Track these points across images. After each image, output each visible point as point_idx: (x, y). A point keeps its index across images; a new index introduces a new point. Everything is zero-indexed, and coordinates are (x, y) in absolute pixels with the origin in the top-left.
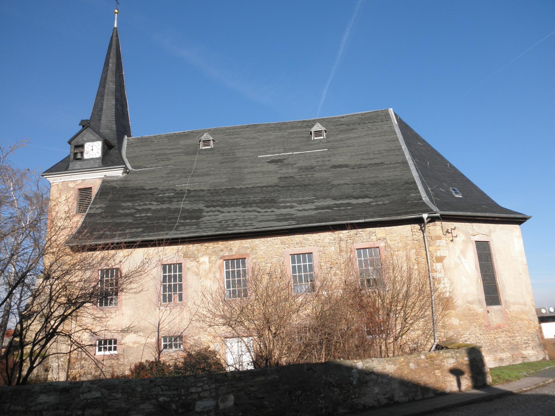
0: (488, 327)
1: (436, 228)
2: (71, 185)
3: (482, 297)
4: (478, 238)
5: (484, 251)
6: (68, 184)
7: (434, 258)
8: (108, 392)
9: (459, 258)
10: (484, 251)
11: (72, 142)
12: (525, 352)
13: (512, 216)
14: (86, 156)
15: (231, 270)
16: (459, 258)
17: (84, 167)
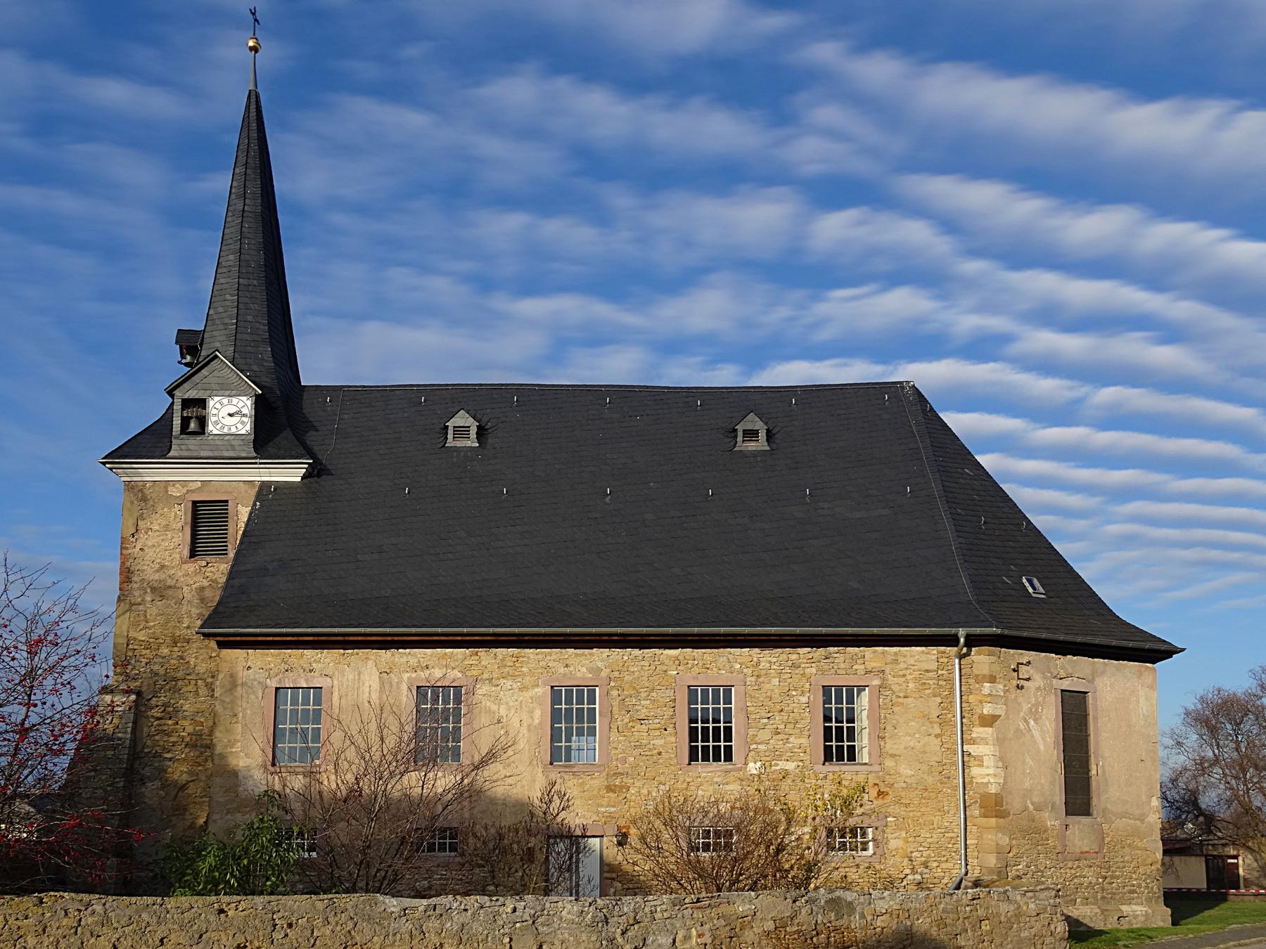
0: (1062, 855)
1: (982, 659)
2: (175, 492)
3: (1059, 798)
4: (1066, 684)
5: (1075, 712)
6: (166, 488)
7: (976, 717)
8: (990, 730)
9: (1026, 721)
10: (1075, 712)
11: (177, 393)
12: (1125, 909)
13: (1148, 646)
14: (211, 428)
15: (699, 706)
16: (1026, 721)
17: (203, 454)
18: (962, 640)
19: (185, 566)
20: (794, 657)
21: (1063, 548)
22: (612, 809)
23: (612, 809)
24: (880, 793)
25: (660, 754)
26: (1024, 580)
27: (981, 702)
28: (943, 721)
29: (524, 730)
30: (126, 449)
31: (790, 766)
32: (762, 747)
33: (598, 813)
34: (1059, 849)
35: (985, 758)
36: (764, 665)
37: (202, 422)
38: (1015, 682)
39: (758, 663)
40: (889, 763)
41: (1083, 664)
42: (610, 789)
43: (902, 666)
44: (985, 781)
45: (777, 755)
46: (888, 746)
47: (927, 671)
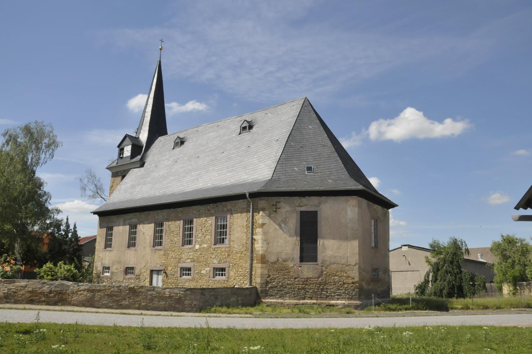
4: (303, 209)
8: (261, 229)
20: (209, 207)
24: (228, 255)
36: (201, 211)
40: (231, 243)
41: (315, 200)
42: (164, 255)
43: (237, 207)
45: (202, 242)
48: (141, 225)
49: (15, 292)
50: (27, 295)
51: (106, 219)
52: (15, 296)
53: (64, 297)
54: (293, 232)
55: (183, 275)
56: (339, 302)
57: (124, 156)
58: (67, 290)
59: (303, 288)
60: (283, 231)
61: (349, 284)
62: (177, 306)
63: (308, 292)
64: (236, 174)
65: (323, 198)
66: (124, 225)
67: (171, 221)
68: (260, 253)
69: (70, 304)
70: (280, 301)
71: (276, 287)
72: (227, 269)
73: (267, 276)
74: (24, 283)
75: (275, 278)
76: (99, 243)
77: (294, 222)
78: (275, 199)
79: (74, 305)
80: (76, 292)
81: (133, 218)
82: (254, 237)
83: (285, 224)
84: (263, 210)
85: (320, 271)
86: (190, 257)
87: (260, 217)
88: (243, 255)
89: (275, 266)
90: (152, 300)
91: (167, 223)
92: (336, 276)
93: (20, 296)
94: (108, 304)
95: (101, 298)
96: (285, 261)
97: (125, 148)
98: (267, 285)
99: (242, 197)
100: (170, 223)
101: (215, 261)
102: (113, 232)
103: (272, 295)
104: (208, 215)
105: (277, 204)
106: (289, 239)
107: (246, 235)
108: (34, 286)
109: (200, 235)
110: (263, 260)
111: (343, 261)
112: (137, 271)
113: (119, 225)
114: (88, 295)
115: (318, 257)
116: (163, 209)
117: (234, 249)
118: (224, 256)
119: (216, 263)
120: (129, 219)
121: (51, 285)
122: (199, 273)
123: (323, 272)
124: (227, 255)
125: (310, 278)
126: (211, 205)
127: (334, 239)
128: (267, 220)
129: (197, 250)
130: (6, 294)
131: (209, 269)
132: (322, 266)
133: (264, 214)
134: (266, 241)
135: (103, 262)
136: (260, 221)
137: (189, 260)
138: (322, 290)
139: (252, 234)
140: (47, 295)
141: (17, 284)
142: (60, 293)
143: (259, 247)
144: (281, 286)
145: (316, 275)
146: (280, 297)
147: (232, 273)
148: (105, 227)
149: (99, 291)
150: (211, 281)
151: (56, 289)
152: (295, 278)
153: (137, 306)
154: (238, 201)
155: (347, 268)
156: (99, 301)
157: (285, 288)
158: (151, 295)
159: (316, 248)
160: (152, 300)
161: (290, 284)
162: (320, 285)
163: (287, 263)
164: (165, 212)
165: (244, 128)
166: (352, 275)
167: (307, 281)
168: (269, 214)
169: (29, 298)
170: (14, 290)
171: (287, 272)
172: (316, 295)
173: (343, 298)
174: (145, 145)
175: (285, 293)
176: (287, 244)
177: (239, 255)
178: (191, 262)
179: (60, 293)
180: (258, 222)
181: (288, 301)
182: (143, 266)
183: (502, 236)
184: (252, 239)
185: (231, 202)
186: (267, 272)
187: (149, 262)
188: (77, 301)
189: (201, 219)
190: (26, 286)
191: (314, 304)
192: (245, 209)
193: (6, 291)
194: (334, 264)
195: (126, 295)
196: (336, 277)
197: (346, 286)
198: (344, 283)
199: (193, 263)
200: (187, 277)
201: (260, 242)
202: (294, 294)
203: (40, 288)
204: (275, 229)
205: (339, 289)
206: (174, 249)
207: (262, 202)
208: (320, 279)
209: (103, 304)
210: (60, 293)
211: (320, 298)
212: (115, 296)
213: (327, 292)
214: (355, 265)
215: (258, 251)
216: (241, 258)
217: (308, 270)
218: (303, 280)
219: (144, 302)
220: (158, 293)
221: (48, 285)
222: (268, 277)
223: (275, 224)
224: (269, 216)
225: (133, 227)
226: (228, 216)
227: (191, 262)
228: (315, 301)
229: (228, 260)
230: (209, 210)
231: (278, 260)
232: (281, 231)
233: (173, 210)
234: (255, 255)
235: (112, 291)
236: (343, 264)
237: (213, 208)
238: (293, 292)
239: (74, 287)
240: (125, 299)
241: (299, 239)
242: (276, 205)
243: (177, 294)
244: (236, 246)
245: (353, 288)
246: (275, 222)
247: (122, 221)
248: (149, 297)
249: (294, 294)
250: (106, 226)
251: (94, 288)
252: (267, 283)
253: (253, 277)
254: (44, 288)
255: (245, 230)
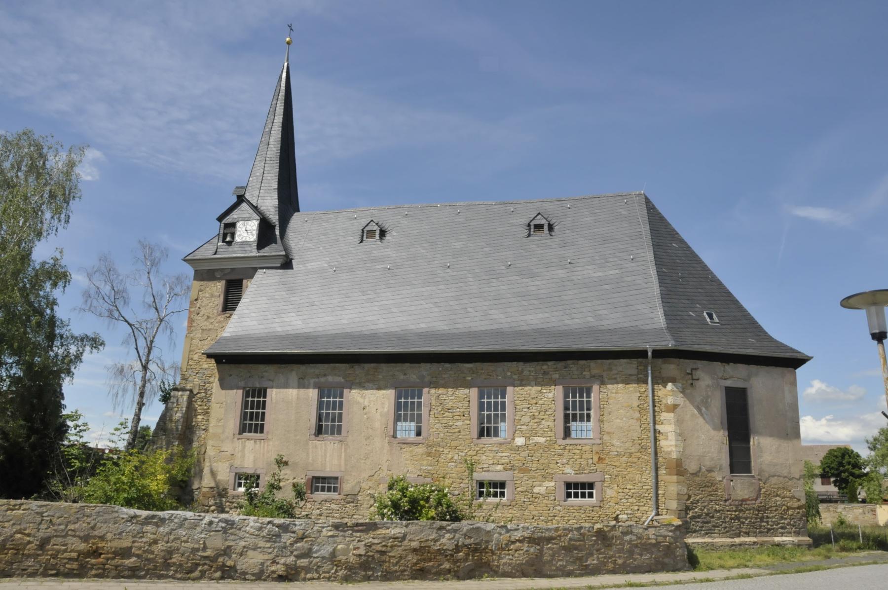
4: (729, 383)
8: (672, 415)
18: (650, 354)
19: (219, 318)
20: (545, 367)
21: (655, 288)
22: (430, 468)
23: (430, 468)
24: (600, 459)
25: (459, 432)
26: (705, 314)
27: (666, 396)
28: (641, 409)
29: (378, 416)
30: (851, 301)
31: (542, 440)
32: (524, 427)
33: (421, 469)
34: (726, 497)
35: (669, 434)
36: (526, 373)
37: (233, 235)
38: (690, 382)
39: (522, 372)
40: (606, 437)
41: (742, 370)
42: (429, 454)
43: (614, 372)
44: (669, 449)
45: (533, 433)
46: (605, 426)
47: (631, 375)
48: (353, 391)
49: (383, 553)
50: (410, 557)
51: (234, 369)
52: (384, 562)
53: (485, 559)
54: (717, 421)
55: (317, 490)
56: (784, 538)
57: (238, 239)
58: (487, 542)
59: (737, 518)
60: (704, 419)
61: (794, 509)
62: (666, 560)
63: (743, 523)
64: (356, 315)
65: (753, 368)
66: (302, 385)
67: (445, 386)
68: (674, 456)
69: (496, 573)
70: (707, 540)
71: (699, 516)
72: (597, 485)
73: (686, 497)
74: (398, 530)
75: (698, 501)
76: (219, 420)
77: (718, 404)
78: (689, 364)
79: (506, 575)
80: (507, 545)
81: (333, 375)
82: (658, 427)
83: (707, 408)
84: (673, 380)
85: (757, 488)
86: (503, 461)
87: (669, 393)
88: (635, 460)
89: (697, 479)
90: (631, 552)
91: (433, 391)
92: (777, 495)
93: (394, 561)
94: (565, 567)
95: (553, 556)
96: (710, 471)
97: (239, 225)
98: (687, 514)
99: (641, 354)
100: (441, 391)
101: (568, 470)
102: (268, 399)
103: (695, 531)
104: (546, 381)
105: (694, 372)
106: (713, 433)
107: (638, 424)
108: (423, 536)
109: (526, 419)
110: (679, 468)
111: (785, 472)
112: (347, 487)
113: (286, 386)
114: (532, 550)
115: (753, 464)
116: (419, 362)
117: (613, 449)
118: (590, 461)
119: (571, 474)
120: (318, 376)
121: (455, 531)
122: (529, 491)
123: (760, 490)
124: (596, 459)
125: (748, 500)
126: (550, 363)
127: (771, 436)
128: (680, 399)
129: (519, 447)
130: (364, 558)
131: (553, 484)
132: (760, 480)
133: (675, 389)
134: (682, 436)
135: (237, 463)
136: (670, 401)
137: (500, 467)
138: (762, 519)
139: (655, 423)
140: (450, 555)
141: (383, 531)
142: (475, 549)
143: (669, 445)
144: (707, 514)
145: (754, 495)
146: (707, 534)
147: (610, 493)
148: (238, 388)
149: (549, 540)
150: (559, 508)
151: (467, 542)
152: (726, 501)
153: (611, 566)
154: (616, 361)
155: (790, 483)
156: (550, 562)
157: (713, 517)
158: (630, 542)
159: (749, 448)
160: (631, 552)
161: (719, 511)
162: (759, 511)
163: (713, 474)
164: (425, 369)
165: (539, 227)
166: (797, 495)
167: (741, 505)
168: (683, 389)
169: (416, 564)
170: (379, 548)
171: (713, 491)
172: (754, 529)
173: (788, 533)
174: (277, 223)
175: (714, 526)
176: (711, 443)
177: (624, 459)
178: (505, 469)
179: (476, 550)
180: (664, 401)
181: (719, 540)
182: (365, 475)
183: (867, 442)
184: (655, 430)
185: (599, 361)
186: (686, 491)
187: (385, 468)
188: (510, 564)
189: (527, 388)
190: (404, 538)
191: (755, 543)
192: (633, 377)
193: (362, 551)
194: (773, 476)
195: (593, 545)
196: (778, 498)
197: (790, 512)
198: (789, 508)
199: (511, 472)
200: (497, 499)
201: (672, 437)
202: (725, 528)
203: (435, 541)
204: (693, 415)
205: (782, 518)
206: (454, 444)
207: (671, 367)
208: (758, 501)
209: (558, 569)
210: (476, 550)
211: (760, 532)
212: (576, 549)
213: (767, 522)
214: (799, 479)
215: (670, 453)
216: (629, 464)
217: (741, 488)
218: (737, 503)
219: (620, 557)
220: (639, 538)
221: (448, 531)
222: (688, 500)
223: (692, 407)
224: (683, 392)
225: (337, 391)
226: (595, 388)
227: (505, 469)
228: (755, 539)
229: (600, 467)
230: (545, 373)
231: (699, 471)
232: (701, 420)
233: (447, 365)
234: (660, 459)
235: (571, 539)
236: (785, 477)
237: (556, 370)
238: (724, 525)
239: (500, 534)
240: (592, 555)
241: (726, 433)
242: (691, 374)
243: (665, 537)
244: (615, 442)
245: (799, 516)
246: (692, 403)
247: (294, 377)
248: (627, 547)
249: (725, 528)
250: (242, 384)
251: (540, 535)
252: (687, 509)
253: (661, 500)
254: (443, 541)
255: (637, 415)
